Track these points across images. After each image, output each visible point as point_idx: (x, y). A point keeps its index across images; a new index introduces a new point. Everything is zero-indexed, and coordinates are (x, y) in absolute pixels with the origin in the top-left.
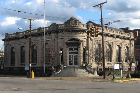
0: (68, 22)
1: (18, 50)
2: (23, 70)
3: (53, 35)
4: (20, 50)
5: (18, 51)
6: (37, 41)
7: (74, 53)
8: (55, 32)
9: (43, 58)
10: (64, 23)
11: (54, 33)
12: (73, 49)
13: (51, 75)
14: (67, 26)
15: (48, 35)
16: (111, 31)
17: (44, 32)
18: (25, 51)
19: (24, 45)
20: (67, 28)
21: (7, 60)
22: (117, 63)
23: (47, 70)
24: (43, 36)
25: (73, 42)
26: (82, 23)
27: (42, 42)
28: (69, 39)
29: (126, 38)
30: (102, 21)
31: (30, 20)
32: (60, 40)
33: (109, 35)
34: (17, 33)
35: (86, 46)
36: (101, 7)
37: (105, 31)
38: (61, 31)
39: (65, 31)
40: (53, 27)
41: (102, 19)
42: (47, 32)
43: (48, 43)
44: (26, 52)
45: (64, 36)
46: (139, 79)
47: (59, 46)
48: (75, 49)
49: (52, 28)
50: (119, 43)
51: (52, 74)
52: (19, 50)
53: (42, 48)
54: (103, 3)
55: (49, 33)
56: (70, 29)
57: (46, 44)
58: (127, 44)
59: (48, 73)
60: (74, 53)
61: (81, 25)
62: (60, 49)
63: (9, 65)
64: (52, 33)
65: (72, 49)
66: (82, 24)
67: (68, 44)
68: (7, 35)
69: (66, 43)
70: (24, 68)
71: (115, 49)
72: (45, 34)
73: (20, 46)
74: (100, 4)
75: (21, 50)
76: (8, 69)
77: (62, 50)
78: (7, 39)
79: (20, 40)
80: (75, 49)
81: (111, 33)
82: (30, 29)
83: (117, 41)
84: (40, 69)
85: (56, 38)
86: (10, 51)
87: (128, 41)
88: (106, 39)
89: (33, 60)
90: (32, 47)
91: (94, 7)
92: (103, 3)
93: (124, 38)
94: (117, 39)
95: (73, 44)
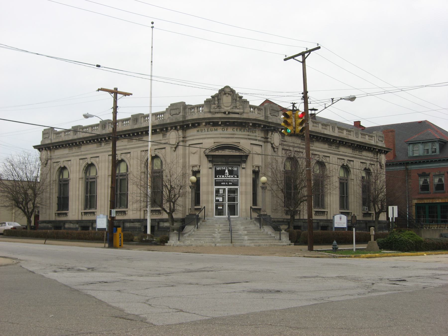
0: (215, 100)
1: (78, 174)
2: (91, 228)
3: (173, 136)
4: (82, 175)
5: (78, 176)
6: (128, 149)
7: (228, 182)
8: (179, 127)
9: (147, 195)
10: (203, 103)
11: (176, 128)
12: (227, 171)
13: (169, 240)
14: (210, 112)
15: (159, 133)
17: (148, 127)
18: (95, 178)
19: (93, 161)
20: (209, 116)
21: (48, 202)
22: (342, 213)
23: (156, 228)
24: (145, 138)
25: (227, 152)
26: (250, 104)
27: (143, 153)
28: (217, 144)
29: (366, 147)
30: (305, 97)
31: (113, 95)
32: (193, 150)
33: (321, 137)
34: (76, 129)
35: (260, 164)
36: (303, 62)
38: (196, 124)
39: (206, 125)
40: (173, 112)
41: (305, 93)
42: (157, 126)
43: (160, 155)
44: (99, 181)
45: (202, 137)
46: (447, 255)
47: (188, 163)
48: (231, 173)
49: (170, 116)
50: (346, 158)
51: (170, 239)
52: (81, 174)
53: (143, 170)
54: (310, 51)
55: (162, 130)
56: (220, 118)
57: (153, 158)
58: (368, 162)
59: (156, 236)
60: (227, 183)
62: (191, 173)
63: (54, 215)
64: (169, 129)
65: (222, 172)
67: (213, 159)
69: (207, 156)
70: (94, 222)
71: (335, 173)
72: (152, 130)
74: (303, 54)
75: (86, 173)
76: (50, 225)
77: (198, 176)
78: (49, 144)
79: (83, 148)
80: (231, 173)
81: (326, 132)
82: (115, 117)
83: (341, 153)
84: (137, 225)
86: (55, 176)
89: (118, 198)
90: (116, 163)
91: (285, 60)
92: (310, 51)
93: (360, 146)
94: (343, 150)
95: (227, 160)
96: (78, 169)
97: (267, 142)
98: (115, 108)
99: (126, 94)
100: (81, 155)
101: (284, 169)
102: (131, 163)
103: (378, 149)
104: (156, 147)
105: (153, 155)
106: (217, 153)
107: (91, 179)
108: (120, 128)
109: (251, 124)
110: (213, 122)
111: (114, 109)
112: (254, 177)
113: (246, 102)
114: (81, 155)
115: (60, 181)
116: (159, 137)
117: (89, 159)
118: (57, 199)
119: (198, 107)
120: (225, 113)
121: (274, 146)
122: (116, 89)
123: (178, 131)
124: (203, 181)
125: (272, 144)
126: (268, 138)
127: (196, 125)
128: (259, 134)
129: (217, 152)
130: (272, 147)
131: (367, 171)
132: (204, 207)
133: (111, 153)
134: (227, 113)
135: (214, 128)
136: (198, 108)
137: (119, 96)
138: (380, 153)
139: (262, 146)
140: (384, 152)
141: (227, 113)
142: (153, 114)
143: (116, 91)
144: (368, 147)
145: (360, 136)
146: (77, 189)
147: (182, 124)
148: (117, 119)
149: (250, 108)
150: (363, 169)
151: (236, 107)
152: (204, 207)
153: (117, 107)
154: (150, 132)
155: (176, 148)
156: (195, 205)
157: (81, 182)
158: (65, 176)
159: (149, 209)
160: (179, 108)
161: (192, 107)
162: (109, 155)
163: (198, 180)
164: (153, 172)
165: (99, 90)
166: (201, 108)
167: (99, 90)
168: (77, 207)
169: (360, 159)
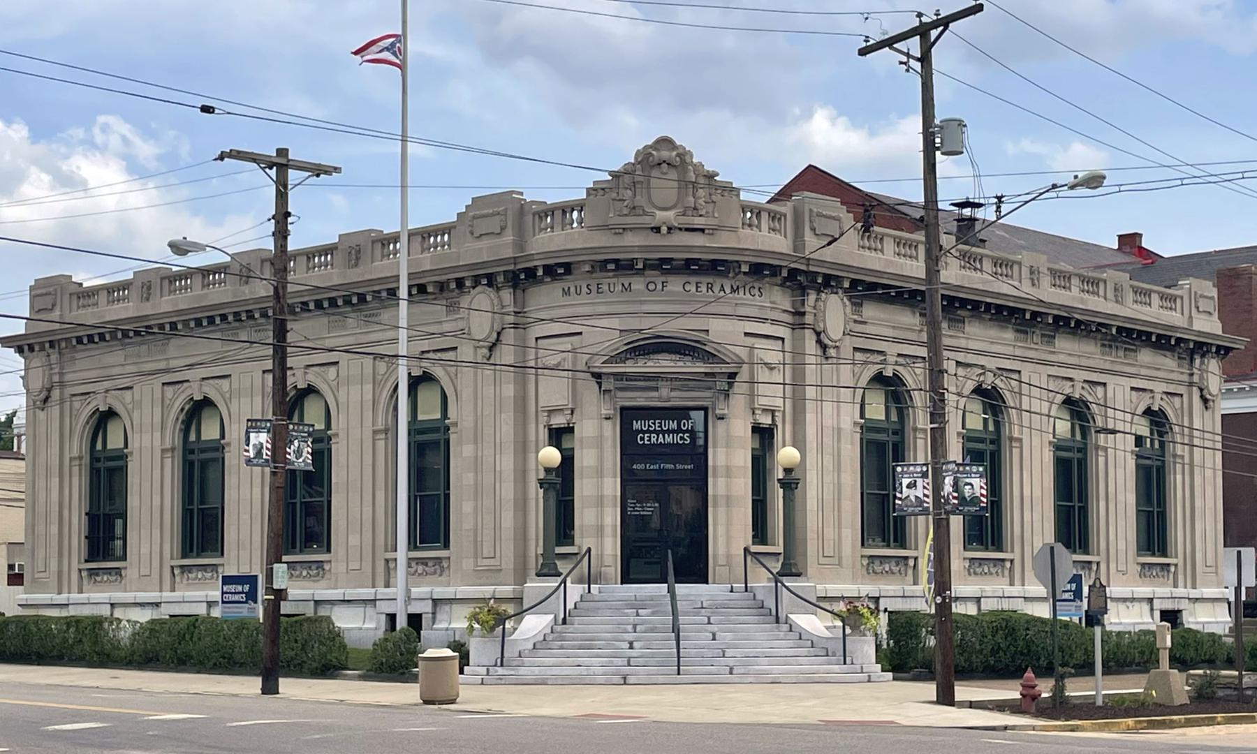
1: (157, 435)
3: (481, 311)
4: (172, 437)
8: (500, 279)
16: (1148, 293)
24: (385, 316)
26: (744, 196)
29: (1149, 334)
33: (988, 305)
36: (925, 59)
37: (953, 274)
50: (1080, 375)
54: (945, 22)
57: (415, 383)
58: (1160, 387)
61: (736, 219)
62: (544, 434)
64: (468, 283)
66: (745, 208)
68: (48, 293)
73: (178, 400)
74: (922, 31)
83: (1062, 358)
85: (510, 336)
87: (908, 319)
88: (962, 343)
90: (290, 403)
91: (863, 52)
92: (945, 22)
94: (1066, 346)
96: (157, 419)
97: (802, 326)
98: (282, 217)
99: (318, 170)
100: (167, 371)
101: (862, 416)
102: (342, 398)
103: (1195, 342)
104: (426, 346)
105: (417, 372)
106: (630, 367)
107: (203, 451)
108: (300, 278)
109: (745, 268)
110: (616, 261)
111: (277, 222)
112: (757, 446)
113: (730, 190)
114: (167, 371)
115: (94, 458)
116: (435, 310)
117: (195, 385)
118: (84, 518)
119: (565, 209)
120: (657, 230)
121: (826, 341)
122: (282, 152)
123: (498, 289)
124: (585, 459)
125: (818, 334)
126: (803, 314)
127: (561, 271)
128: (778, 300)
129: (629, 363)
130: (819, 342)
131: (1156, 418)
132: (589, 550)
133: (269, 365)
134: (664, 229)
135: (622, 280)
136: (564, 212)
137: (293, 176)
138: (1203, 356)
139: (783, 339)
140: (1217, 352)
141: (664, 229)
142: (412, 234)
143: (283, 161)
144: (1159, 336)
145: (1130, 296)
146: (157, 485)
147: (511, 267)
148: (291, 247)
149: (744, 212)
150: (1140, 410)
151: (695, 209)
152: (589, 550)
153: (289, 214)
154: (403, 292)
155: (491, 349)
156: (559, 544)
157: (168, 462)
158: (114, 441)
159: (402, 553)
160: (502, 211)
161: (546, 212)
162: (264, 372)
163: (568, 460)
164: (415, 428)
165: (221, 158)
166: (575, 214)
167: (221, 158)
168: (156, 548)
169: (1131, 375)
